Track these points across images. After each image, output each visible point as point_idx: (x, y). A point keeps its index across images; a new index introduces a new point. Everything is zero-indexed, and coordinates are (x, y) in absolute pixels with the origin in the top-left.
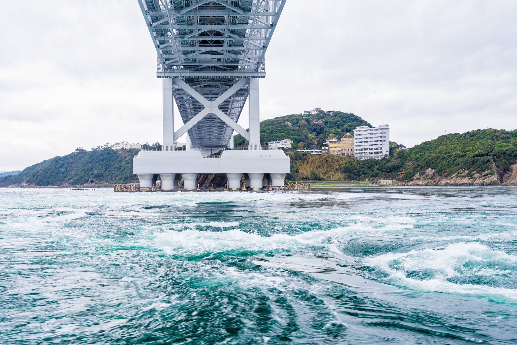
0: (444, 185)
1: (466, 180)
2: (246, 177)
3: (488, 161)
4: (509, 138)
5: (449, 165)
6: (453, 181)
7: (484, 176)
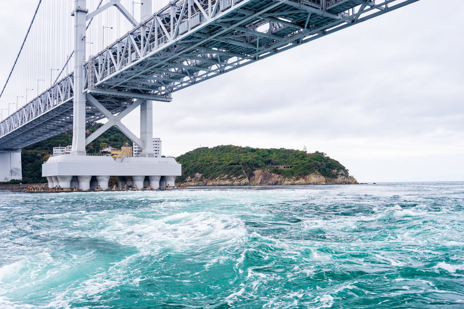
0: (211, 186)
1: (227, 182)
2: (147, 179)
3: (241, 168)
4: (246, 152)
5: (212, 171)
6: (218, 183)
7: (240, 179)
